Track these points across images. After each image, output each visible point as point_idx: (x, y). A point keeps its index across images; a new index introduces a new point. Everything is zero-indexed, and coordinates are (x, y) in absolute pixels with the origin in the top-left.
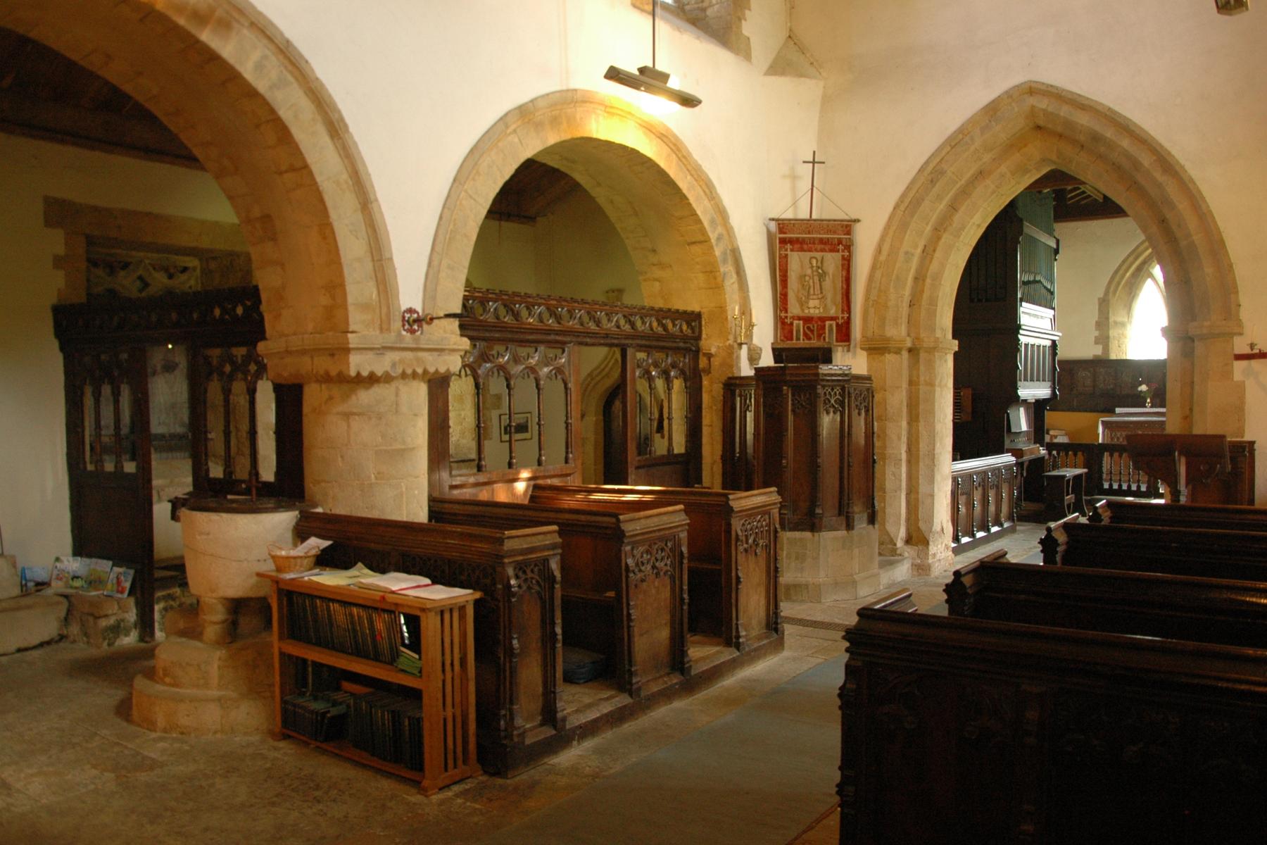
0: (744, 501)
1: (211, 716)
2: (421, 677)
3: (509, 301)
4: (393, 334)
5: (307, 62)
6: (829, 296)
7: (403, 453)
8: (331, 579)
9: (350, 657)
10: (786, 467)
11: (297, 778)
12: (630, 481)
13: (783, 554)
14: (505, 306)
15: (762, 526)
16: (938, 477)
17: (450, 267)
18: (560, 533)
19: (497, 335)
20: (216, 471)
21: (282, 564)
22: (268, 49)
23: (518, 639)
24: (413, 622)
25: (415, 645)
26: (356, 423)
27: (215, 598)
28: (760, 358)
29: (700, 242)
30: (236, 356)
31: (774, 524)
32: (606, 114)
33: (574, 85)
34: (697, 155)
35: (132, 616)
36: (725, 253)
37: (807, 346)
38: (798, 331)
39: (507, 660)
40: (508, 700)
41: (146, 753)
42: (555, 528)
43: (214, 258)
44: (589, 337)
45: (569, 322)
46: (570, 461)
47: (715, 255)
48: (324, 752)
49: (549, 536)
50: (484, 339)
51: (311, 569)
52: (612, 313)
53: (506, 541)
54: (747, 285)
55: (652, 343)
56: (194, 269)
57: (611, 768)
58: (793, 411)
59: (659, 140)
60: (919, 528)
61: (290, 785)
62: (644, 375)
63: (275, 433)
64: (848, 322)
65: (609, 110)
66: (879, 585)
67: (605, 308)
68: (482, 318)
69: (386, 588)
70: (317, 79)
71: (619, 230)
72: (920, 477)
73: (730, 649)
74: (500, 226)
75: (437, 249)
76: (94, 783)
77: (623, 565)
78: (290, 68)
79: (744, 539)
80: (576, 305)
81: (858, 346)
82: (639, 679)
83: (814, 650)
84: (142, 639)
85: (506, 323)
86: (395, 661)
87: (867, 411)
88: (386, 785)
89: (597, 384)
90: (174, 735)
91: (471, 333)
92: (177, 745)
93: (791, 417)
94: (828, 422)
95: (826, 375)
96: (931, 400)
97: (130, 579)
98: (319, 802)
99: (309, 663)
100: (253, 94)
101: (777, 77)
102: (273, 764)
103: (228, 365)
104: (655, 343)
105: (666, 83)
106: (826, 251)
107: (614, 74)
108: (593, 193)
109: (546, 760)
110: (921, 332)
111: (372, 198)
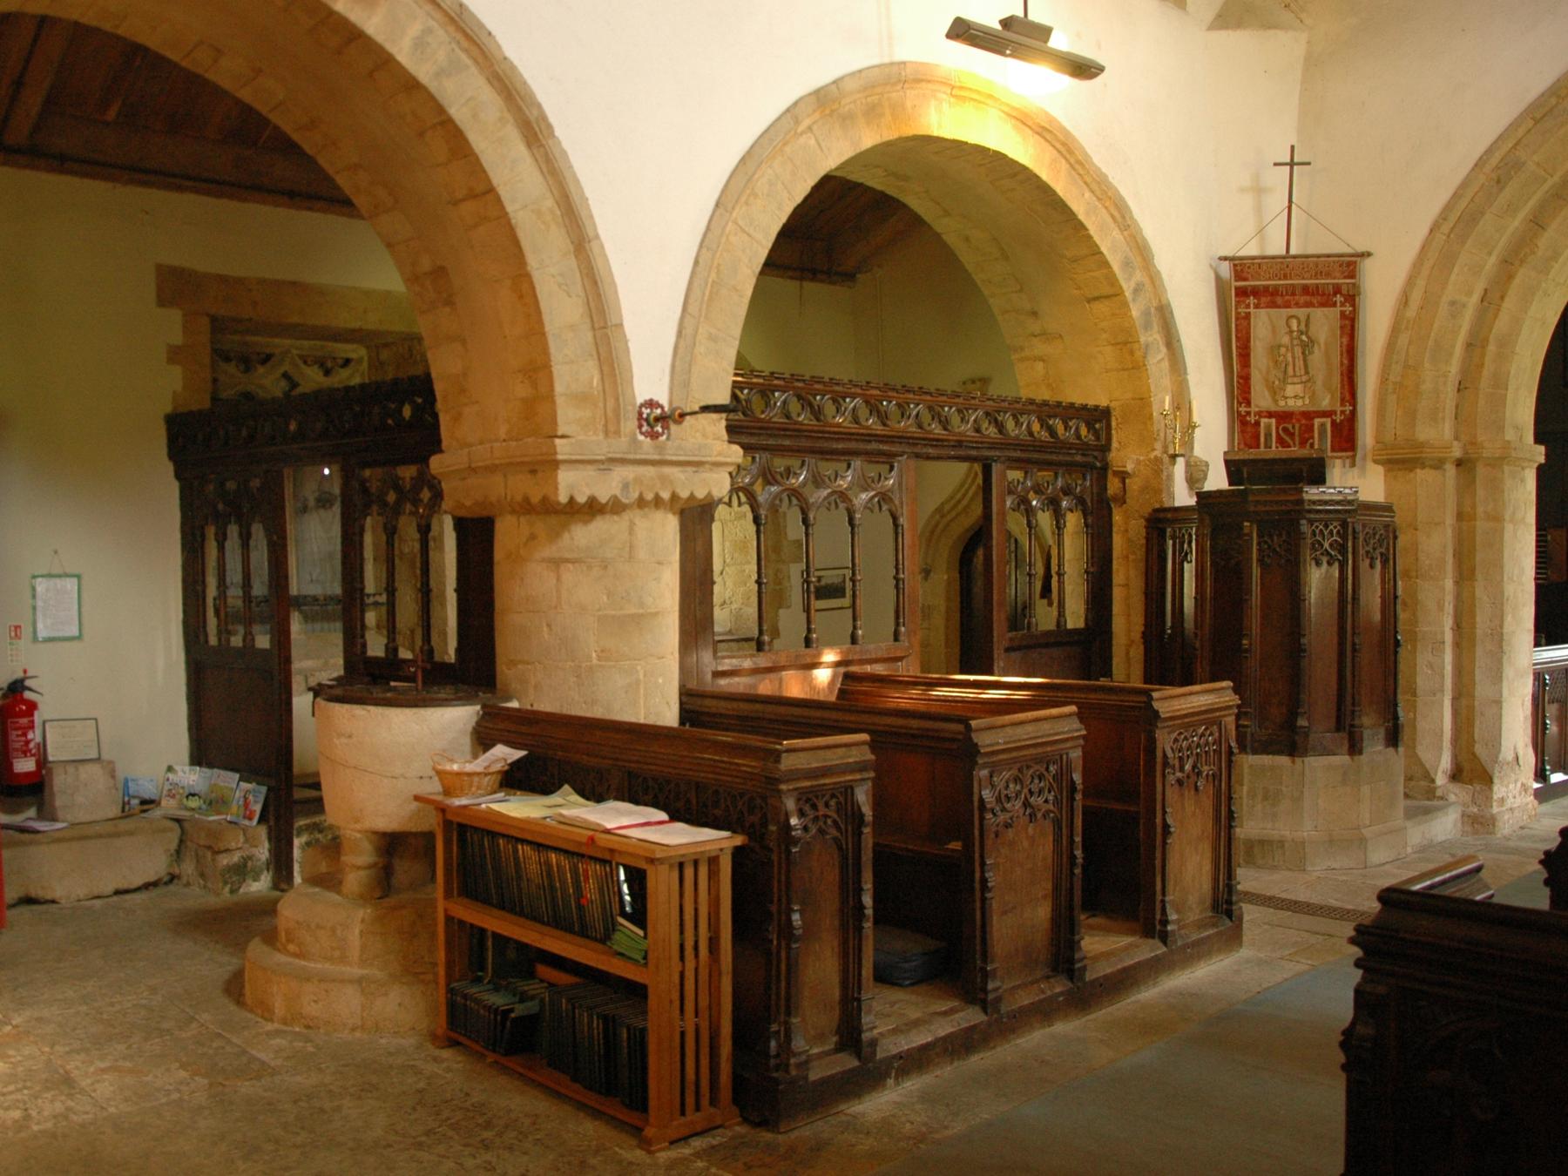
0: (1176, 702)
1: (347, 1004)
2: (646, 964)
3: (805, 390)
4: (623, 439)
5: (490, 34)
6: (1320, 379)
7: (641, 620)
8: (521, 808)
9: (546, 929)
10: (1247, 651)
11: (461, 1108)
12: (996, 671)
13: (1243, 792)
14: (799, 397)
15: (1207, 744)
16: (1508, 672)
17: (712, 338)
18: (874, 746)
19: (787, 442)
20: (376, 647)
21: (452, 782)
22: (433, 18)
23: (802, 912)
24: (637, 878)
25: (639, 916)
26: (569, 575)
27: (359, 832)
28: (1205, 478)
29: (1107, 297)
30: (403, 479)
31: (1227, 740)
32: (952, 100)
33: (901, 54)
34: (1100, 159)
35: (263, 852)
36: (1147, 313)
37: (1284, 457)
38: (1268, 435)
39: (783, 944)
40: (783, 1010)
41: (254, 1052)
42: (865, 737)
43: (386, 345)
44: (932, 446)
45: (899, 422)
46: (902, 638)
47: (1131, 316)
48: (504, 1070)
49: (854, 751)
50: (765, 449)
51: (495, 792)
52: (967, 409)
53: (784, 755)
55: (1030, 455)
56: (360, 361)
57: (946, 1128)
58: (1261, 561)
59: (1037, 137)
60: (1474, 754)
61: (448, 1119)
62: (1019, 504)
63: (456, 590)
64: (1352, 418)
65: (957, 91)
66: (1405, 847)
67: (957, 400)
68: (763, 416)
69: (598, 825)
70: (505, 58)
71: (978, 282)
72: (1477, 672)
73: (1151, 941)
74: (801, 286)
75: (691, 309)
76: (179, 1091)
77: (976, 798)
78: (465, 44)
79: (1177, 763)
80: (911, 396)
81: (1369, 457)
82: (998, 984)
83: (1292, 950)
84: (276, 886)
85: (801, 424)
86: (610, 939)
87: (1385, 562)
88: (589, 1129)
89: (948, 525)
90: (297, 1029)
91: (745, 440)
92: (298, 1044)
93: (1256, 571)
94: (1318, 580)
95: (1314, 502)
96: (1496, 543)
97: (262, 798)
98: (487, 1148)
99: (489, 934)
100: (412, 85)
101: (1230, 32)
102: (429, 1084)
103: (392, 492)
104: (1036, 456)
105: (1046, 41)
106: (1314, 306)
107: (962, 31)
108: (938, 226)
109: (842, 1107)
111: (591, 234)
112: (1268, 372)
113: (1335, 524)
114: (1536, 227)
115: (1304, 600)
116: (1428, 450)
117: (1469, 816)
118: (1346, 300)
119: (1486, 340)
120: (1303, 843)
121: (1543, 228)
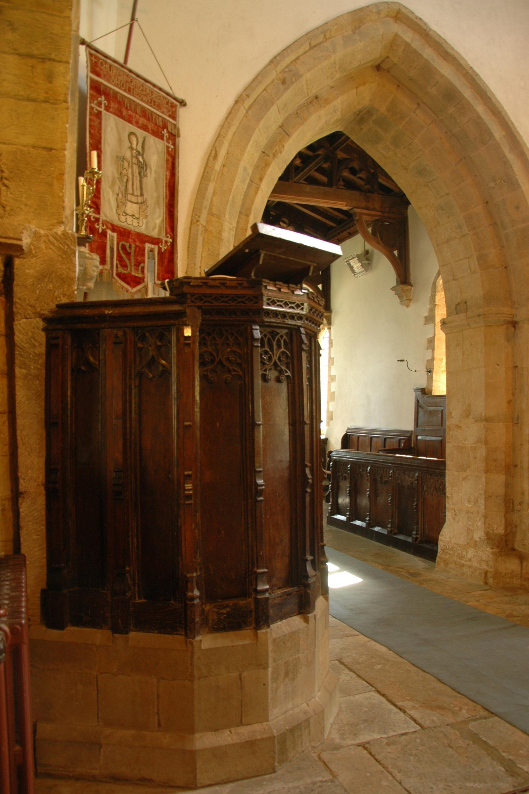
64: (173, 246)
114: (284, 132)
121: (288, 135)
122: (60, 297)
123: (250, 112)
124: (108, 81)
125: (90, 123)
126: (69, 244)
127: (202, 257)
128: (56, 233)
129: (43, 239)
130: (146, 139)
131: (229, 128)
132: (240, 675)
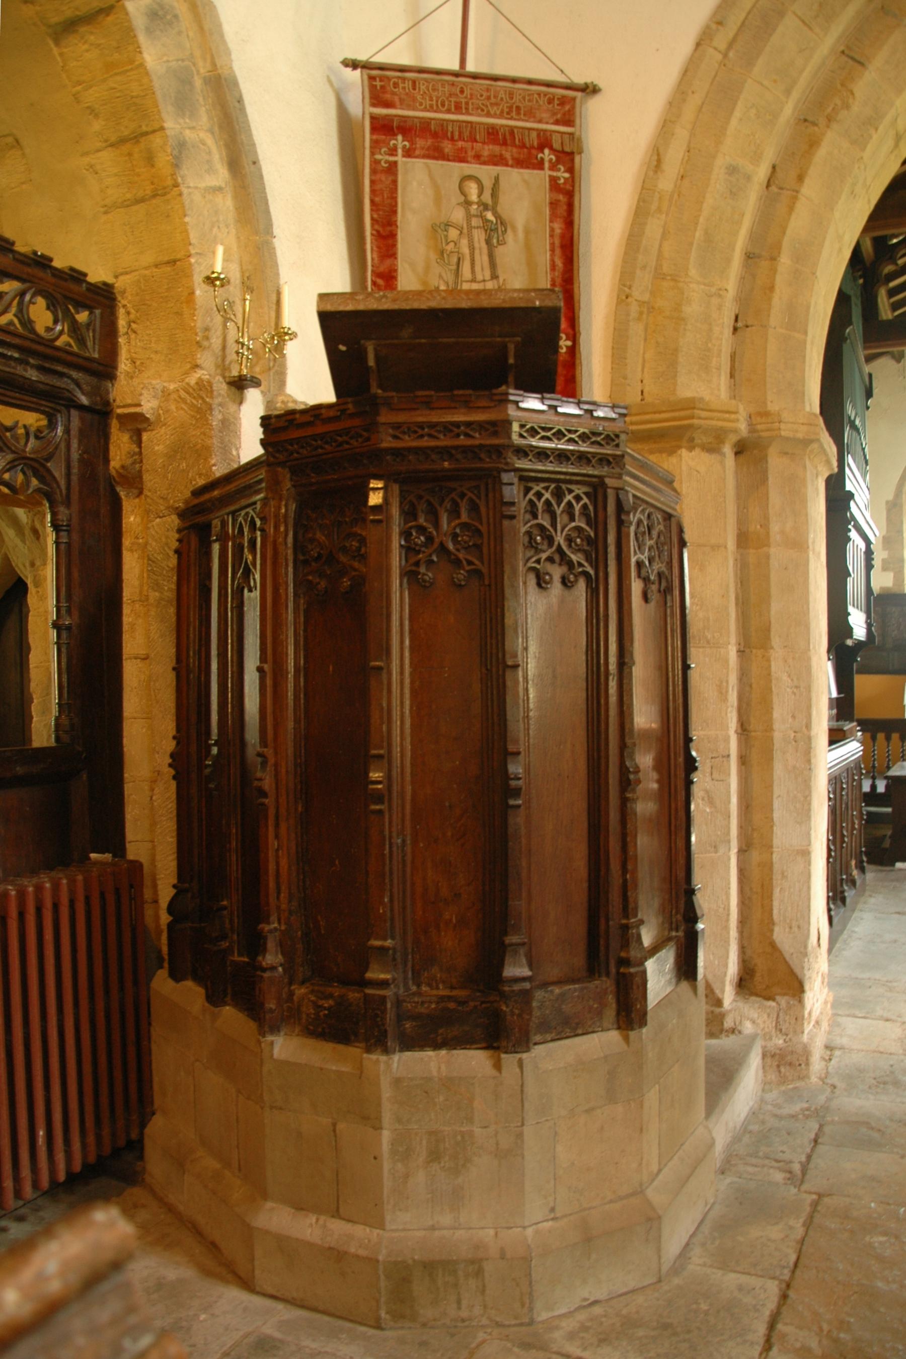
10: (379, 798)
47: (142, 65)
54: (267, 212)
58: (411, 575)
60: (773, 945)
72: (776, 804)
110: (770, 397)
112: (427, 268)
113: (579, 490)
114: (851, 62)
115: (516, 667)
116: (704, 414)
117: (773, 1056)
118: (558, 161)
119: (777, 247)
120: (527, 1260)
122: (195, 480)
123: (731, 54)
124: (410, 107)
125: (371, 186)
126: (204, 396)
127: (644, 361)
128: (188, 384)
129: (174, 396)
130: (501, 178)
131: (684, 100)
132: (334, 1125)
